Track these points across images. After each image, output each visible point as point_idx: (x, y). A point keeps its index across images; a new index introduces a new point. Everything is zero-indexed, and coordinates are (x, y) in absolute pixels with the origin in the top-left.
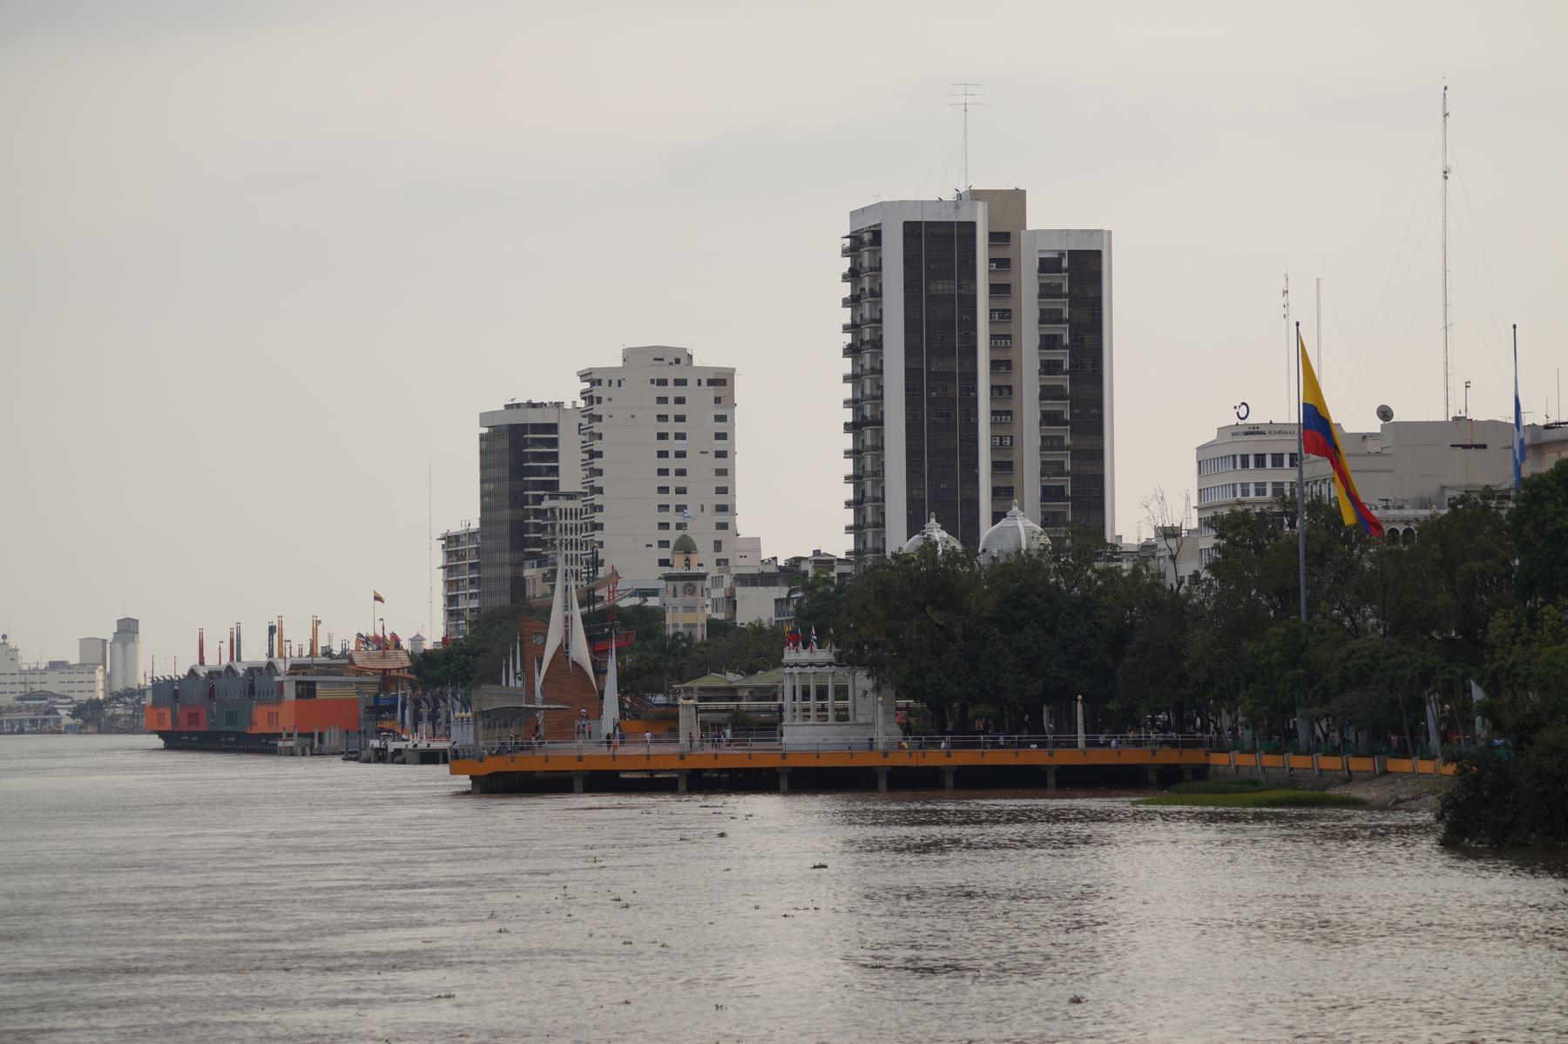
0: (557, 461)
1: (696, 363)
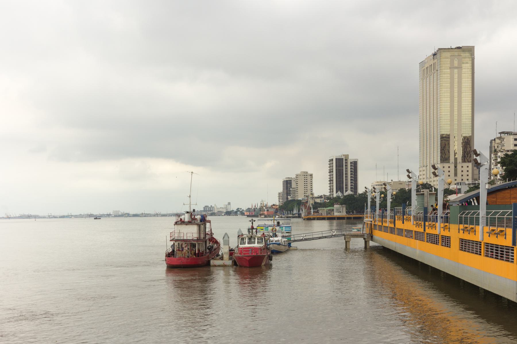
0: (486, 211)
1: (308, 173)
